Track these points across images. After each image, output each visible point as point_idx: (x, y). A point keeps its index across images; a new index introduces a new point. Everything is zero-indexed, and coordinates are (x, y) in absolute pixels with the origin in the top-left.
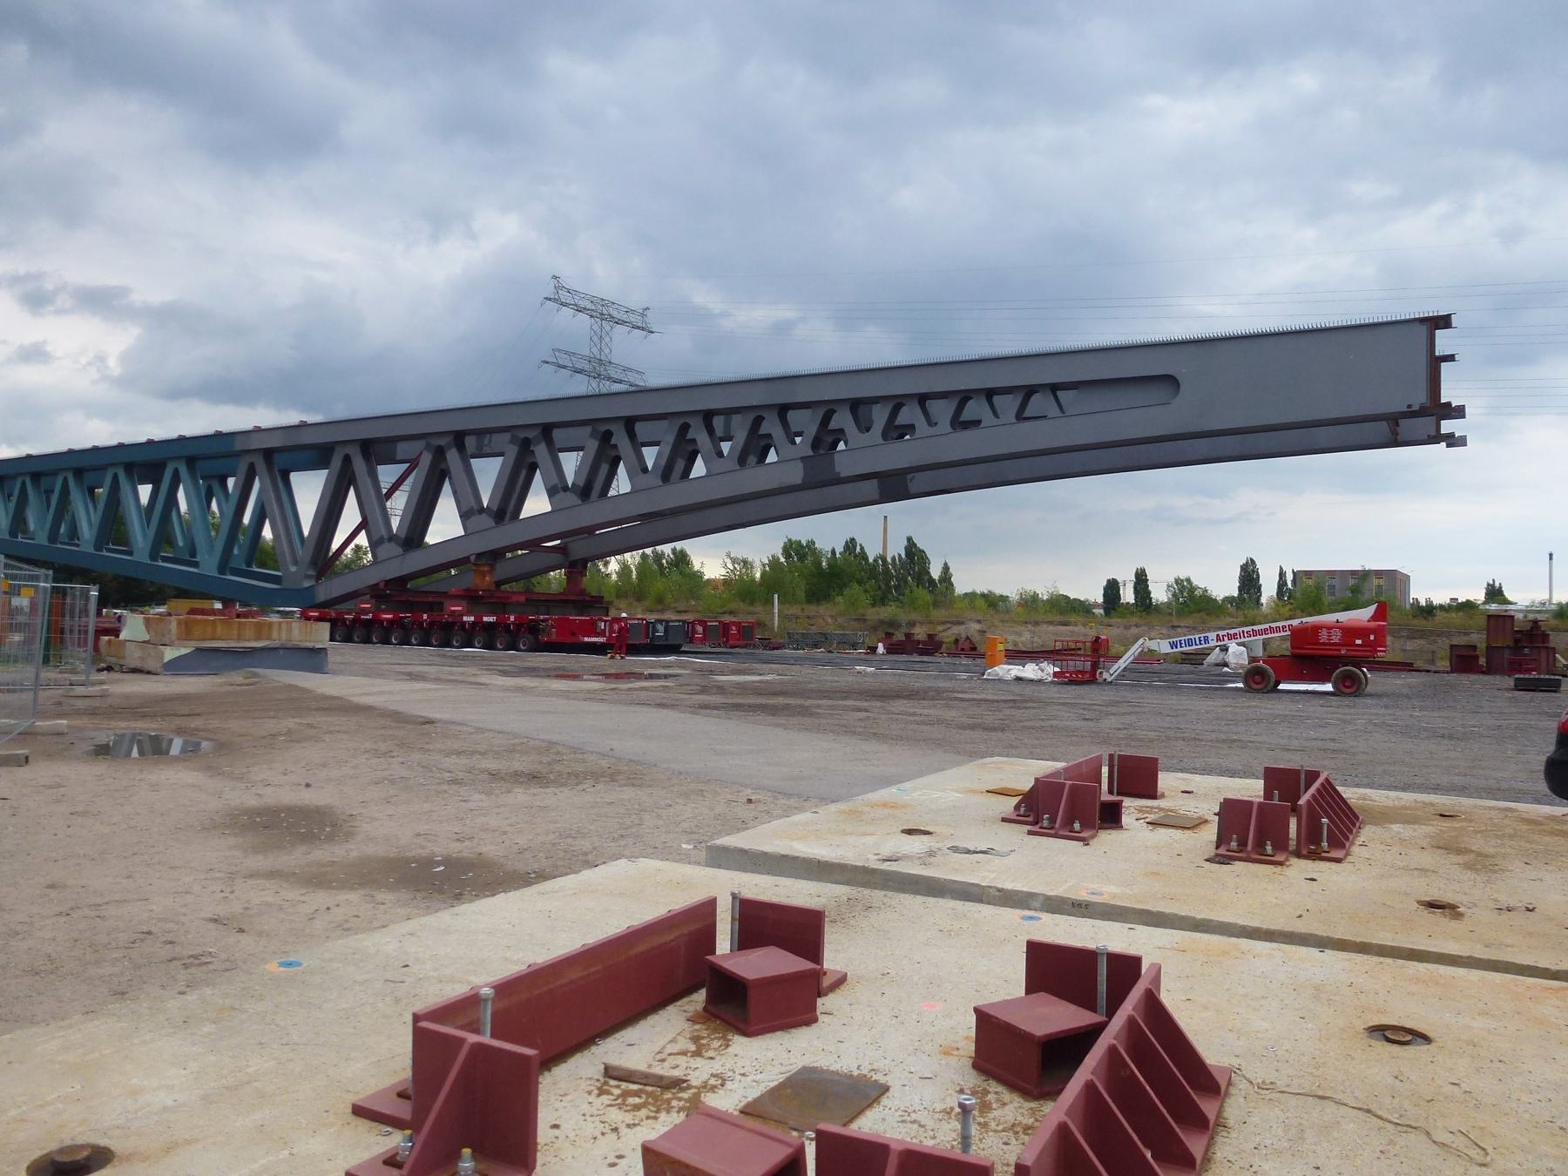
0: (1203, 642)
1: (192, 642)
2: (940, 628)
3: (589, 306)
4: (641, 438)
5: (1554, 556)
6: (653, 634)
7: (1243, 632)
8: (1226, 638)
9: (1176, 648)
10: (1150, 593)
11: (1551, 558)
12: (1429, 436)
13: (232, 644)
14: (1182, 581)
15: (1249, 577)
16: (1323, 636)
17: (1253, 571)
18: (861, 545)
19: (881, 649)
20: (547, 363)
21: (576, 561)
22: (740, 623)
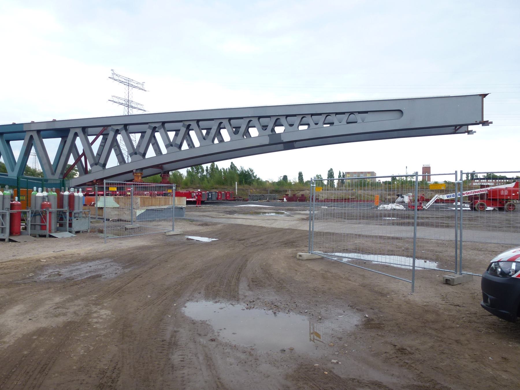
0: (451, 197)
1: (145, 207)
2: (296, 192)
3: (124, 81)
4: (201, 127)
5: (407, 167)
6: (208, 197)
7: (471, 192)
8: (466, 194)
9: (449, 197)
10: (303, 179)
11: (406, 168)
12: (465, 131)
13: (158, 207)
14: (318, 176)
15: (331, 174)
16: (502, 193)
17: (332, 172)
18: (216, 165)
19: (285, 200)
20: (110, 101)
21: (166, 171)
22: (230, 192)
